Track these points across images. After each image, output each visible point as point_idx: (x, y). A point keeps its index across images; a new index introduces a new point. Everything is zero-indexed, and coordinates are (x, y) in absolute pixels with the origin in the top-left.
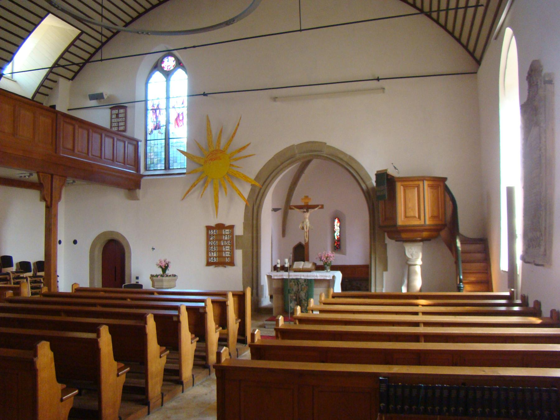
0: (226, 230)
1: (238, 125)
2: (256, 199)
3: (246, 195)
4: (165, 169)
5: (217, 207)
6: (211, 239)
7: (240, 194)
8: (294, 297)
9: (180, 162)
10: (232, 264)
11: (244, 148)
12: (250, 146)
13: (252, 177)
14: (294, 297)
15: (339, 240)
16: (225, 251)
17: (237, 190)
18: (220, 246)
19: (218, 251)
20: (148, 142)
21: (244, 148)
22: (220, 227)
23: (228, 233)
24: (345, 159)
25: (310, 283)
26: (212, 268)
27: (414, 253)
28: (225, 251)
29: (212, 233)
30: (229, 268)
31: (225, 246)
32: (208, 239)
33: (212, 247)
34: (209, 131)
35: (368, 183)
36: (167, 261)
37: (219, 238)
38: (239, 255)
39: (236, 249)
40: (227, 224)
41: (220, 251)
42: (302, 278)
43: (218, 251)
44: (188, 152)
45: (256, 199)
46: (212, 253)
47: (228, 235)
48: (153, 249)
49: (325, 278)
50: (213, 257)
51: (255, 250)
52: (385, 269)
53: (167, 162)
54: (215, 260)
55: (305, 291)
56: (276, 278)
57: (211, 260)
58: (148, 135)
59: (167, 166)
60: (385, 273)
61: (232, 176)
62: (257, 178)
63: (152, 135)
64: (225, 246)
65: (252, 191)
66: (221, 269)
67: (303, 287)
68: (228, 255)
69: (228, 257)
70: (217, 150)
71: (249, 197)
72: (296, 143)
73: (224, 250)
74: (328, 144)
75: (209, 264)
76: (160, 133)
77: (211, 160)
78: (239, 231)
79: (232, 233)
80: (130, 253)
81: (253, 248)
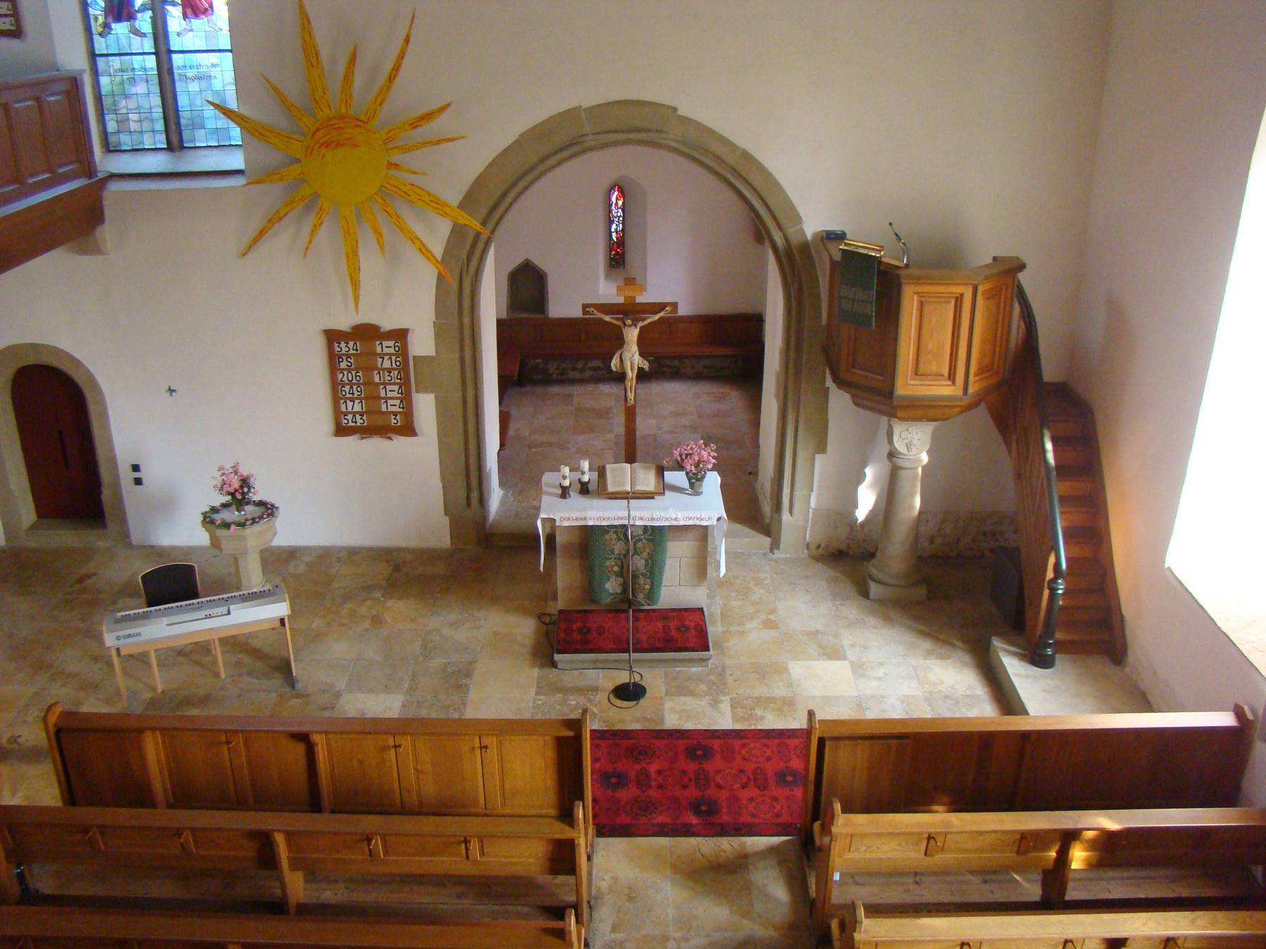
0: (385, 343)
1: (407, 40)
2: (469, 258)
3: (438, 250)
4: (170, 148)
5: (356, 285)
6: (343, 365)
7: (424, 250)
8: (616, 569)
9: (222, 149)
10: (408, 429)
11: (428, 117)
12: (448, 111)
13: (454, 197)
14: (616, 569)
15: (621, 242)
16: (387, 399)
17: (414, 239)
18: (369, 383)
19: (366, 398)
20: (101, 63)
21: (428, 117)
22: (367, 333)
23: (392, 351)
24: (731, 159)
25: (656, 535)
26: (351, 441)
27: (915, 442)
28: (387, 399)
29: (344, 349)
30: (401, 442)
31: (385, 384)
32: (333, 368)
33: (347, 388)
34: (310, 54)
35: (791, 231)
36: (244, 471)
37: (366, 363)
38: (425, 407)
39: (417, 391)
40: (387, 325)
41: (373, 399)
42: (638, 523)
43: (366, 398)
44: (245, 112)
45: (469, 258)
46: (350, 404)
47: (390, 355)
48: (171, 391)
49: (699, 523)
50: (354, 414)
51: (470, 394)
52: (821, 448)
53: (173, 127)
54: (359, 421)
55: (645, 555)
56: (566, 524)
57: (348, 421)
58: (96, 38)
59: (175, 140)
60: (818, 457)
61: (393, 196)
62: (468, 202)
63: (111, 38)
64: (385, 384)
65: (458, 231)
66: (376, 442)
67: (640, 544)
68: (396, 409)
69: (395, 414)
70: (342, 117)
71: (448, 251)
72: (586, 104)
73: (383, 394)
74: (680, 112)
75: (341, 430)
76: (137, 32)
77: (327, 145)
78: (423, 344)
79: (403, 352)
80: (102, 403)
81: (464, 390)
